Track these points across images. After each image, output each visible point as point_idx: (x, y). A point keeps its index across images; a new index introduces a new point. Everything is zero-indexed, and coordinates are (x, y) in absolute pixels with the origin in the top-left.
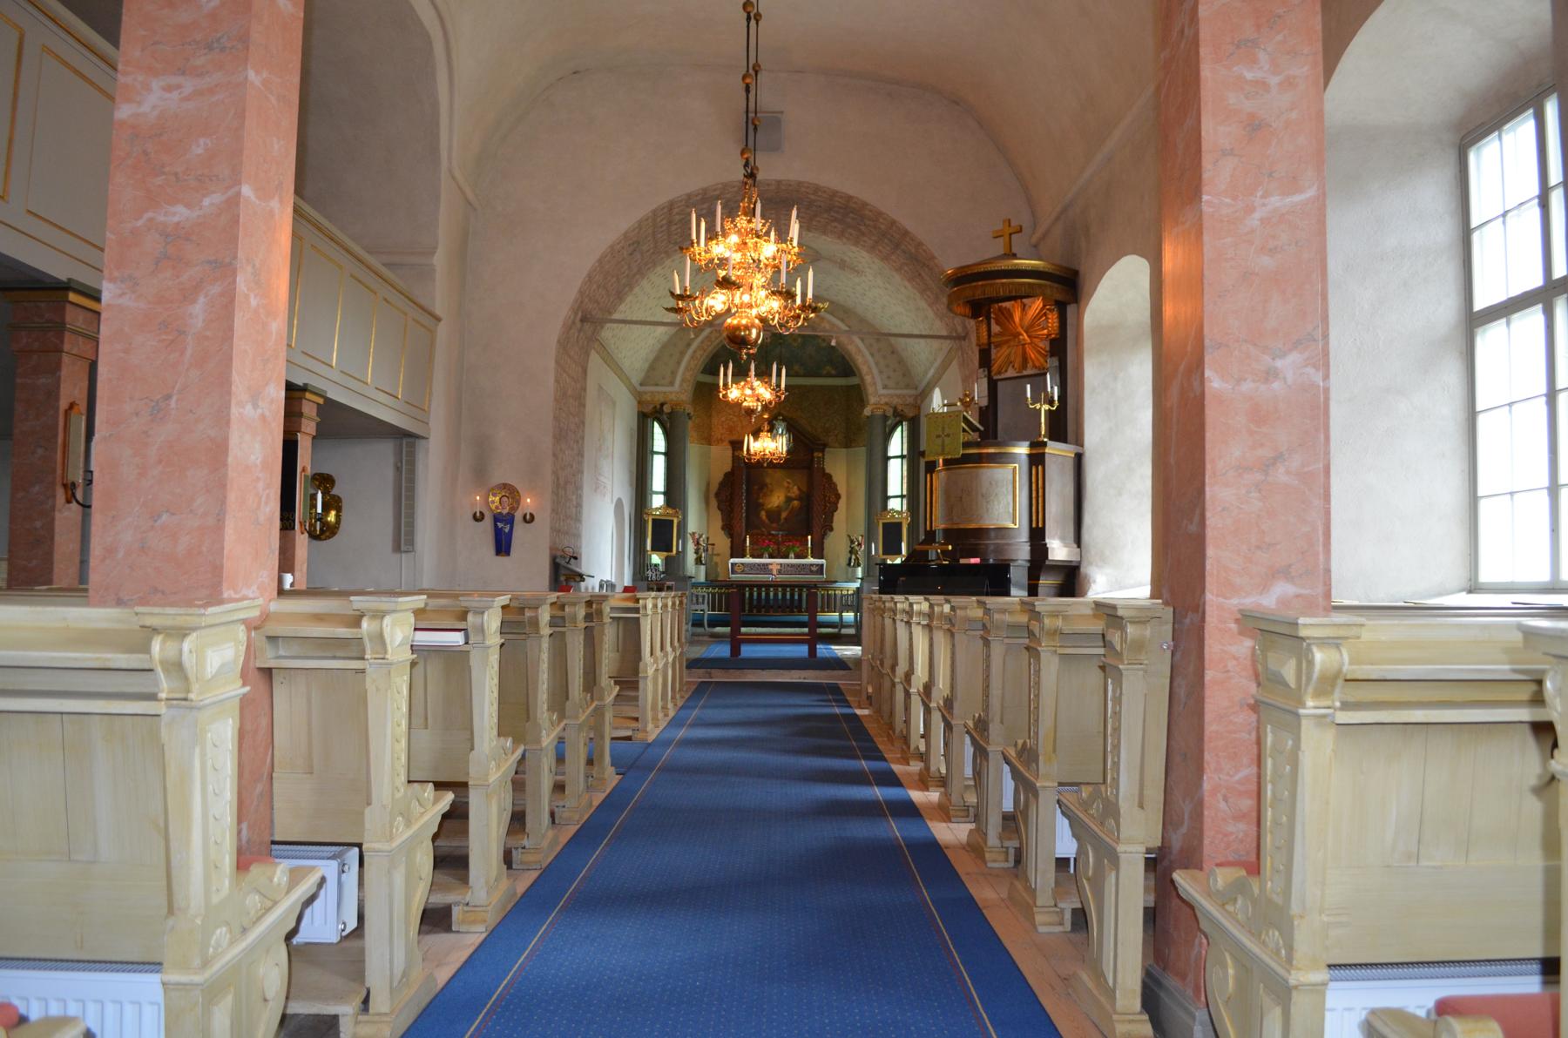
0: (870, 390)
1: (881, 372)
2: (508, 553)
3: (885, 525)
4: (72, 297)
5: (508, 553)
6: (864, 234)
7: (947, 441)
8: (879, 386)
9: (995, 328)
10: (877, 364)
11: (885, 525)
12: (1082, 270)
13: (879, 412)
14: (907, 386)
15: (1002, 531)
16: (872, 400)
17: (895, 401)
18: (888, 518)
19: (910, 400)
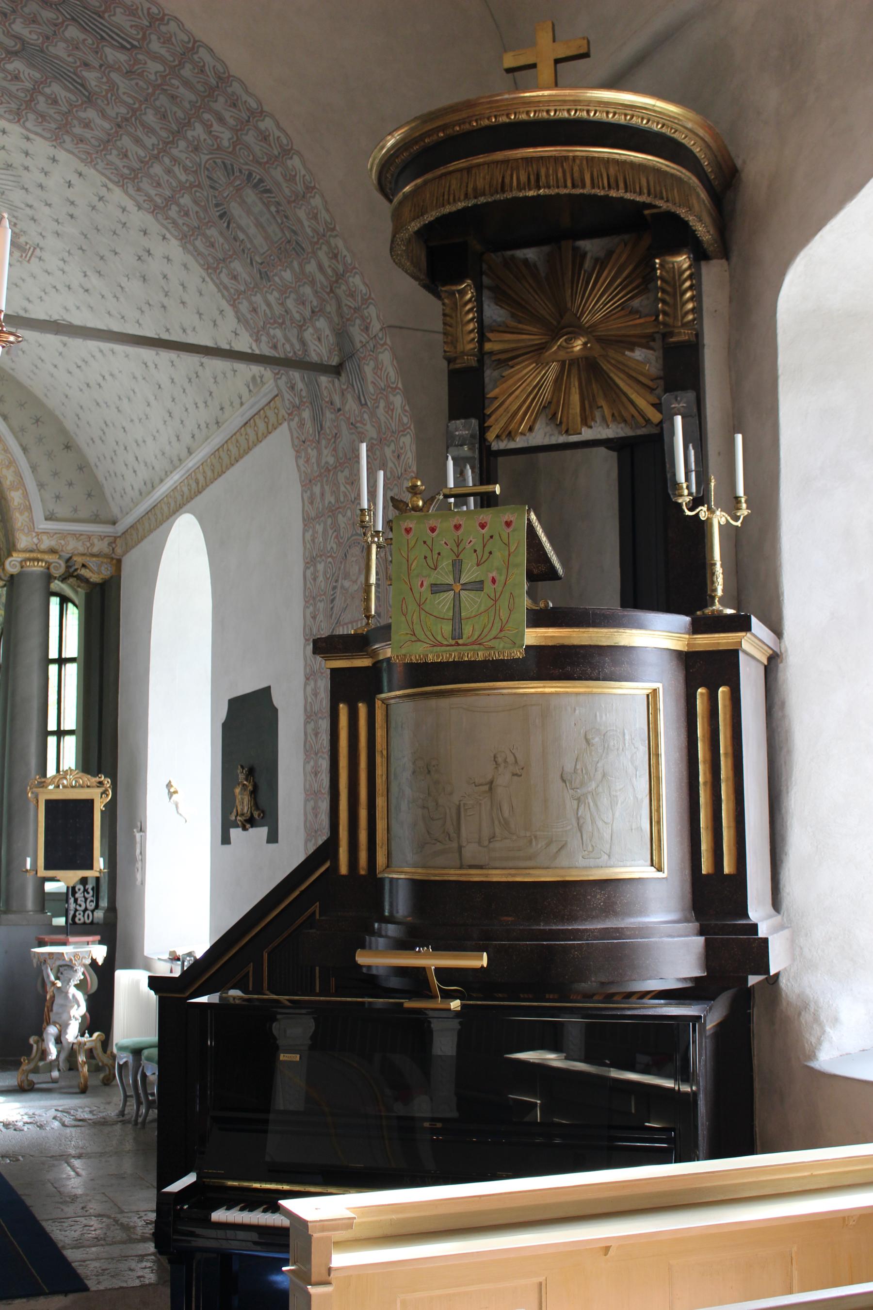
0: (19, 520)
1: (41, 486)
2: (276, 841)
3: (48, 803)
4: (706, 867)
5: (276, 841)
6: (90, 99)
7: (471, 601)
8: (38, 513)
9: (493, 312)
10: (34, 468)
11: (48, 803)
12: (739, 163)
13: (37, 568)
14: (96, 519)
15: (609, 892)
16: (23, 541)
17: (72, 546)
18: (52, 792)
19: (100, 546)
